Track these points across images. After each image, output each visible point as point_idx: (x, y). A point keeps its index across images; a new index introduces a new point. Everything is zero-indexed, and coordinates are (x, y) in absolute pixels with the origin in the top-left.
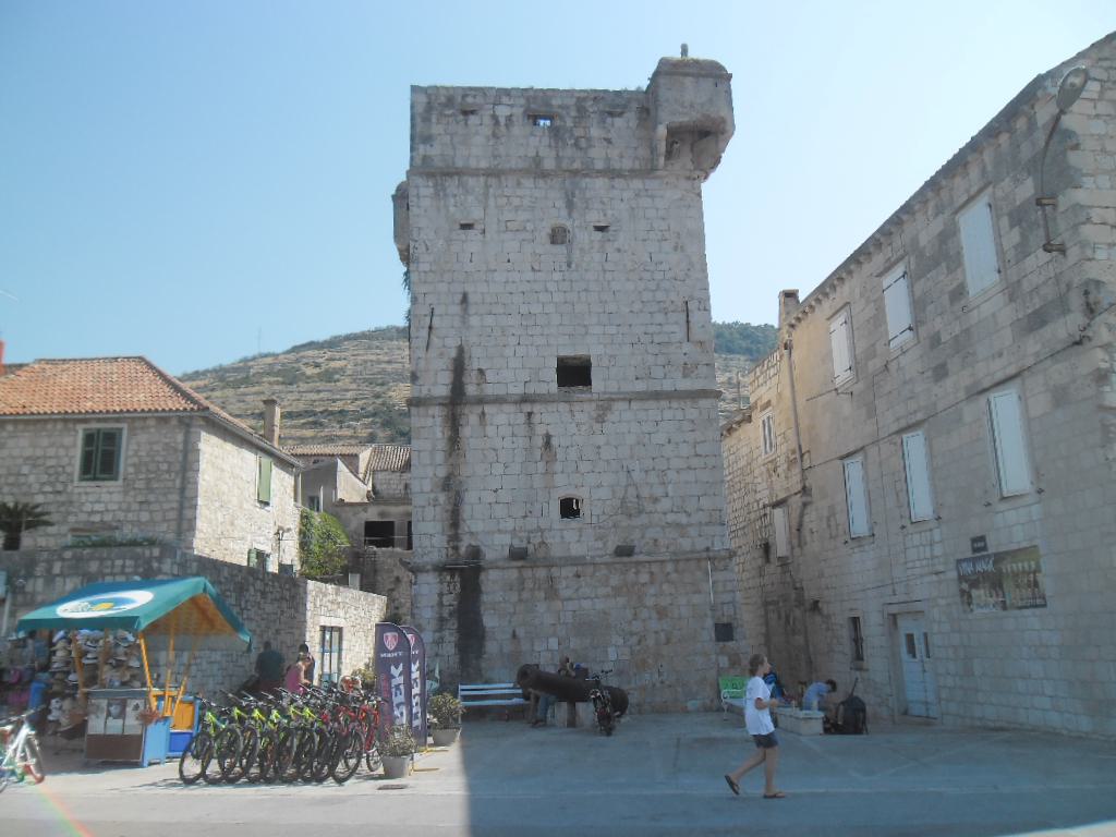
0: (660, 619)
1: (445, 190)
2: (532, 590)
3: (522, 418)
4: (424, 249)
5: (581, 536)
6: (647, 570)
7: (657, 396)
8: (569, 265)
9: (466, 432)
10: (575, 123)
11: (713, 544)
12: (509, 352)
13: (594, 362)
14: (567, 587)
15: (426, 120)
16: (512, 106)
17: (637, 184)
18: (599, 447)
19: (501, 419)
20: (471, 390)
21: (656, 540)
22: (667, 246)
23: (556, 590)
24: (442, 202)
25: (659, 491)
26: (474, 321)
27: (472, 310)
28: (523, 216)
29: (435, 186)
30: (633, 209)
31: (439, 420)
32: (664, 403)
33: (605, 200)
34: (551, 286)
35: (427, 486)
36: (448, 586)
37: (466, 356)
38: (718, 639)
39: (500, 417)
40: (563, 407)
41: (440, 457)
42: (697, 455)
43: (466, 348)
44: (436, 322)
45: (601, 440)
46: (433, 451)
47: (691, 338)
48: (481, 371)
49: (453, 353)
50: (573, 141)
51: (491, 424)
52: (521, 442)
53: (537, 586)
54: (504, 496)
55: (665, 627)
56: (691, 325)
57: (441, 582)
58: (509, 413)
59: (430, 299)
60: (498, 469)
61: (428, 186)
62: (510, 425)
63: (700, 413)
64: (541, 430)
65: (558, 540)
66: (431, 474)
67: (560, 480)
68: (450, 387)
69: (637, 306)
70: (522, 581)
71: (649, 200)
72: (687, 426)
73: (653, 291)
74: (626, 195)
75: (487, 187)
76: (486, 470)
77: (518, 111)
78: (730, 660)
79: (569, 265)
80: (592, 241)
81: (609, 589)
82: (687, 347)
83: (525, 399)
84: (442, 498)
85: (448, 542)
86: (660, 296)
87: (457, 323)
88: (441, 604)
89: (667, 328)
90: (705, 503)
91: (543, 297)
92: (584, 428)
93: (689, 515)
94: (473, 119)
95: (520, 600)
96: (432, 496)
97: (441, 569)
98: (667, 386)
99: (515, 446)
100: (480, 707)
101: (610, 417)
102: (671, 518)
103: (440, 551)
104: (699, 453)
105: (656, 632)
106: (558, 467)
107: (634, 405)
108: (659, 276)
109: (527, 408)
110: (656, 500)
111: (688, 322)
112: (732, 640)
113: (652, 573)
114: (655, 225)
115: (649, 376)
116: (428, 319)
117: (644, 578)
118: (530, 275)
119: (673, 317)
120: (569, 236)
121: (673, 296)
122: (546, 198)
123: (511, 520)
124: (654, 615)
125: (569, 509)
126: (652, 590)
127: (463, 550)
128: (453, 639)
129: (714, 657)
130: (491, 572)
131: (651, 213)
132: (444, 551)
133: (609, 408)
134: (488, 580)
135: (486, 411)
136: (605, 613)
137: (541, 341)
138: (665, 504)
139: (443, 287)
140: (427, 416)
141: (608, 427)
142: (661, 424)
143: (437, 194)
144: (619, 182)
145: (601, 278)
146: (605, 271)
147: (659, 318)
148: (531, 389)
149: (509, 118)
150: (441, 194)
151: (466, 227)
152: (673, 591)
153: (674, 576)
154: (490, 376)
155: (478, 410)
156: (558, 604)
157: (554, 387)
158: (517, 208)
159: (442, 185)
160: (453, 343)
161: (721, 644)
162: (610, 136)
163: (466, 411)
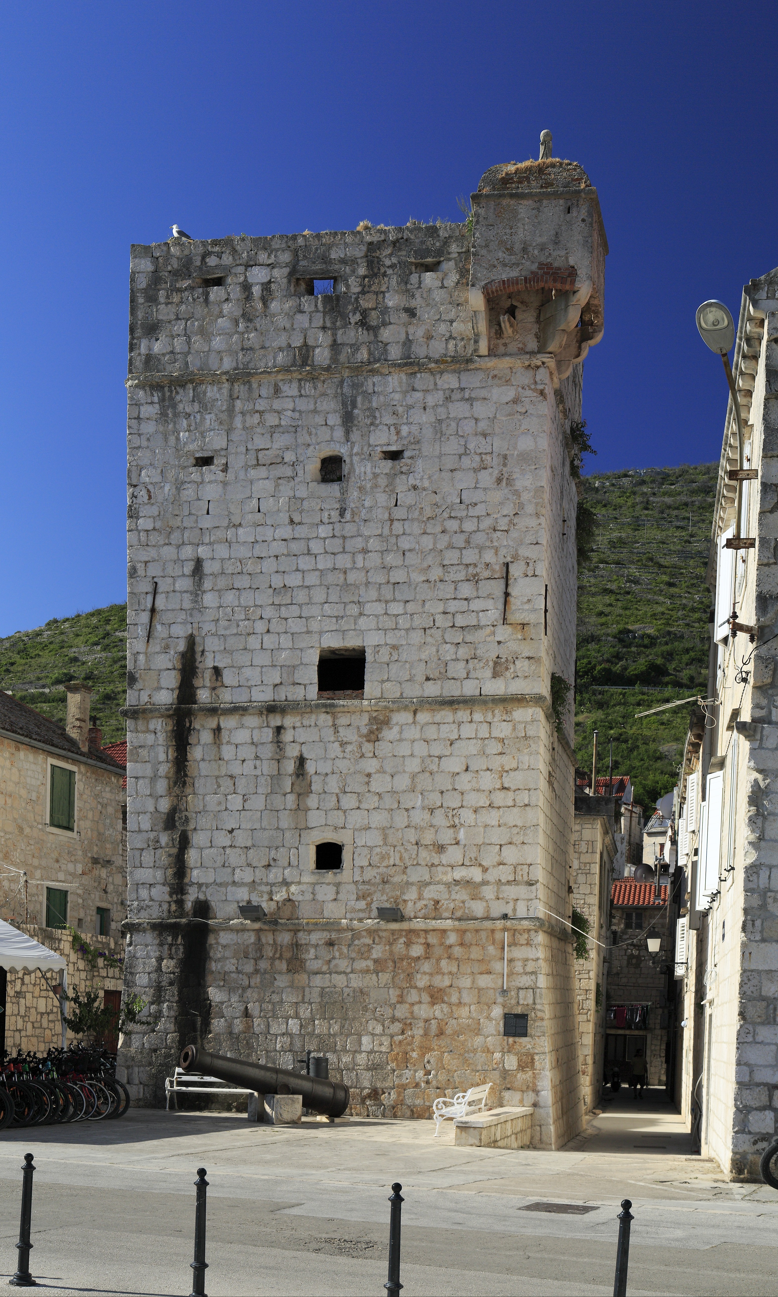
0: (433, 1004)
1: (174, 406)
2: (273, 959)
3: (268, 735)
4: (146, 497)
5: (338, 893)
6: (422, 940)
7: (451, 703)
8: (342, 515)
9: (196, 753)
10: (362, 285)
11: (515, 910)
12: (254, 643)
13: (369, 657)
14: (316, 958)
15: (152, 299)
16: (271, 266)
17: (449, 381)
18: (369, 775)
19: (242, 736)
20: (203, 696)
21: (437, 902)
22: (486, 478)
23: (302, 962)
24: (171, 426)
25: (446, 837)
26: (209, 599)
27: (207, 584)
28: (281, 440)
29: (162, 400)
30: (440, 421)
31: (161, 738)
32: (463, 714)
33: (400, 410)
34: (316, 547)
35: (146, 825)
36: (170, 949)
37: (198, 649)
38: (507, 1033)
39: (288, 807)
40: (324, 719)
41: (162, 786)
42: (504, 788)
43: (198, 640)
44: (161, 603)
45: (371, 765)
46: (154, 779)
47: (511, 618)
48: (217, 671)
49: (182, 646)
50: (358, 317)
51: (228, 742)
52: (267, 768)
53: (277, 955)
54: (242, 839)
55: (438, 1014)
56: (511, 599)
57: (161, 944)
58: (253, 729)
59: (154, 570)
60: (235, 802)
61: (152, 403)
62: (253, 743)
63: (514, 729)
64: (293, 752)
65: (309, 896)
66: (152, 809)
67: (315, 819)
68: (176, 692)
69: (436, 573)
70: (259, 946)
71: (467, 406)
72: (493, 748)
73: (461, 549)
74: (431, 400)
75: (232, 398)
76: (220, 803)
77: (280, 274)
78: (519, 1061)
79: (342, 515)
80: (376, 476)
81: (370, 963)
82: (503, 633)
83: (272, 709)
84: (164, 839)
85: (171, 895)
86: (470, 556)
87: (187, 605)
88: (159, 969)
89: (476, 605)
90: (511, 855)
91: (305, 563)
92: (349, 748)
93: (485, 870)
94: (216, 293)
95: (257, 971)
96: (152, 835)
97: (160, 928)
98: (469, 689)
99: (258, 772)
100: (199, 1095)
101: (389, 734)
102: (459, 874)
103: (160, 906)
104: (506, 785)
105: (426, 1021)
106: (312, 801)
107: (423, 717)
108: (469, 526)
109: (276, 720)
110: (441, 848)
111: (507, 594)
112: (525, 1035)
113: (428, 945)
114: (471, 446)
115: (444, 676)
116: (150, 598)
117: (417, 950)
118: (286, 532)
119: (488, 587)
120: (346, 469)
121: (489, 556)
122: (315, 411)
123: (249, 870)
124: (426, 998)
125: (329, 857)
126: (426, 967)
127: (189, 905)
128: (172, 1013)
129: (497, 1055)
130: (222, 934)
131: (468, 427)
132: (165, 907)
133: (386, 722)
134: (218, 943)
135: (222, 725)
136: (361, 991)
137: (295, 626)
138: (454, 855)
139: (168, 552)
140: (148, 731)
141: (383, 748)
142: (457, 745)
143: (163, 414)
144: (423, 380)
145: (386, 531)
146: (392, 521)
147: (466, 590)
148: (282, 694)
149: (267, 286)
150: (170, 412)
151: (205, 461)
152: (455, 970)
153: (457, 951)
154: (228, 678)
155: (212, 723)
156: (302, 978)
157: (313, 691)
158: (273, 430)
159: (171, 398)
160: (181, 631)
161: (511, 1040)
162: (413, 304)
163: (197, 725)
